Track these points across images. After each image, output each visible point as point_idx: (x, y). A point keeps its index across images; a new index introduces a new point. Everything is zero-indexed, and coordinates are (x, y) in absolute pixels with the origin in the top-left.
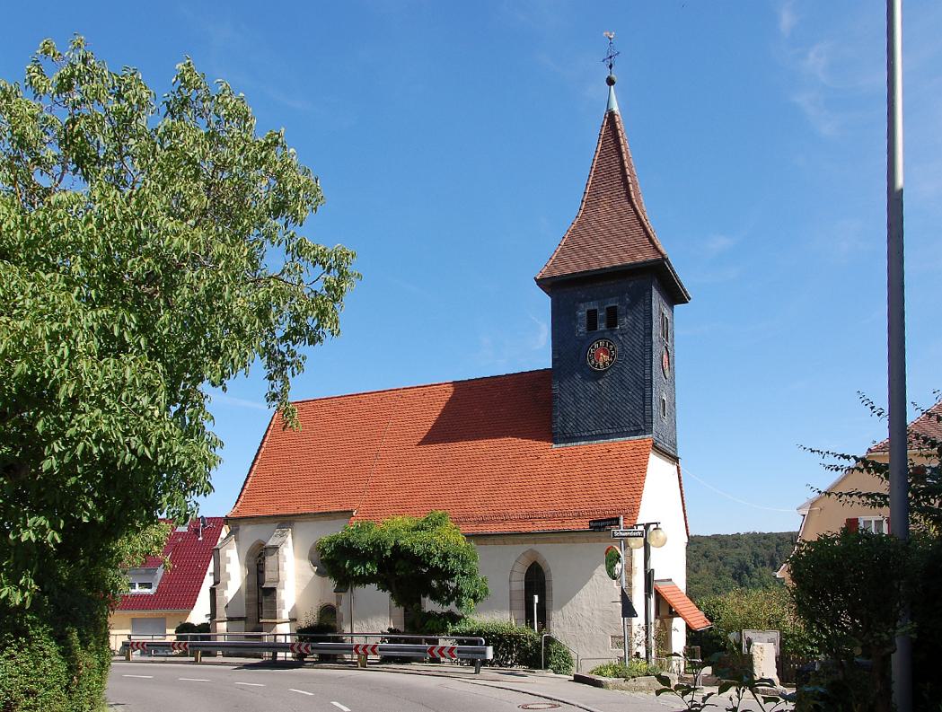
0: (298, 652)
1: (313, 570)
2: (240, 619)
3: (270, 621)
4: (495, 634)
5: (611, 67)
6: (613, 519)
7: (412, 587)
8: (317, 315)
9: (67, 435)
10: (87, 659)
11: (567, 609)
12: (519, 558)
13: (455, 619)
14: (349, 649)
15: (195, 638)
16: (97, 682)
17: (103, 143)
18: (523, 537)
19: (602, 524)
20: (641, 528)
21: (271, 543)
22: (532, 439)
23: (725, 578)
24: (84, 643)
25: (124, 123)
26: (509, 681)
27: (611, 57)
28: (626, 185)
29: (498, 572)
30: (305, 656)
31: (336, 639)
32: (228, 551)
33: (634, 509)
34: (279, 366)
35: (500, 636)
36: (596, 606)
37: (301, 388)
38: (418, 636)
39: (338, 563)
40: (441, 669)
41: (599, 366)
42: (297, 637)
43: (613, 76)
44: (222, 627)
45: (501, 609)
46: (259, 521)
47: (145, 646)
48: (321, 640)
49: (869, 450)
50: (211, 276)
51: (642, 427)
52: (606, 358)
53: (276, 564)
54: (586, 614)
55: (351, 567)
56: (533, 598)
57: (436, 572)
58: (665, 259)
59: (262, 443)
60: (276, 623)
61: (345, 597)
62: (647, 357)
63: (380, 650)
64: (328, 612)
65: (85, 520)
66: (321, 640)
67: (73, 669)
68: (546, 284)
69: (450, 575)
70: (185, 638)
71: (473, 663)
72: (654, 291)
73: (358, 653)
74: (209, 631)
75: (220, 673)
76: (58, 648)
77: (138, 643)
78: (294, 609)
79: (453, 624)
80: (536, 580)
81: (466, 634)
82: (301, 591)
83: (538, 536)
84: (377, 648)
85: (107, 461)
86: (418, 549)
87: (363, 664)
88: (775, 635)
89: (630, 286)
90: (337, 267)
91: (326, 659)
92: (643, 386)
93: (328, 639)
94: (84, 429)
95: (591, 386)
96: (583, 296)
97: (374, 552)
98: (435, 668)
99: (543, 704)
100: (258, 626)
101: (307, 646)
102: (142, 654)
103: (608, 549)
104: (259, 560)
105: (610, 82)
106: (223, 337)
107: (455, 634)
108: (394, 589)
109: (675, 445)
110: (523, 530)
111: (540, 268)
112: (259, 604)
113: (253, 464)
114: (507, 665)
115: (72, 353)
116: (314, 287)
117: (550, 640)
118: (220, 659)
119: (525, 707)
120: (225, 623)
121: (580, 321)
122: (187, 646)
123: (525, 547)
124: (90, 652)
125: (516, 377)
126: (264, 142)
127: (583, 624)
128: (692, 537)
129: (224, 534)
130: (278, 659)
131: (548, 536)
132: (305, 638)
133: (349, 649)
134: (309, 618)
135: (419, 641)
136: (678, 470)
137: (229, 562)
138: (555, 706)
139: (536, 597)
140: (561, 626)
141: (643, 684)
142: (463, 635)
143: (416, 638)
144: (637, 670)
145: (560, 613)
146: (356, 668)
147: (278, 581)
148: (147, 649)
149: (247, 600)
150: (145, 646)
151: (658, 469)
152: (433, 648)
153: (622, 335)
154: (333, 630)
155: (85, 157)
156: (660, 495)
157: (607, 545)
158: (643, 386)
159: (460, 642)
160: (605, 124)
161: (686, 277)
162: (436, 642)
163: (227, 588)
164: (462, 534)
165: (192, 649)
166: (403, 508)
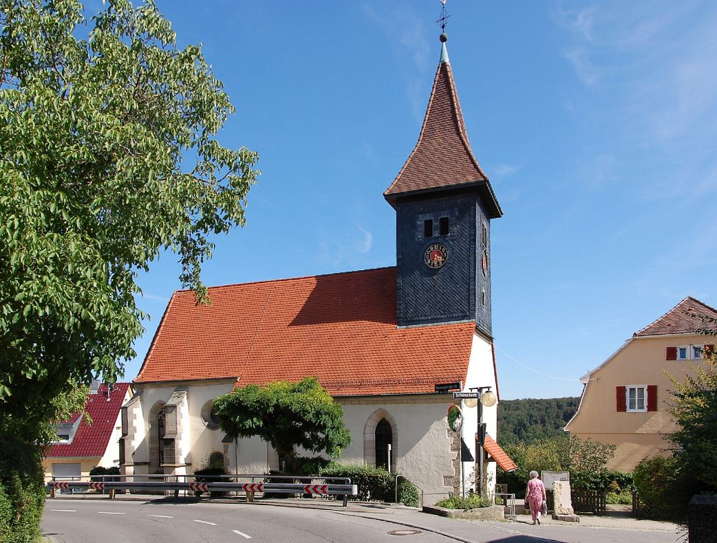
0: (196, 490)
1: (205, 425)
2: (145, 463)
3: (170, 465)
4: (357, 474)
5: (443, 27)
6: (453, 384)
7: (285, 439)
8: (226, 206)
9: (16, 299)
10: (27, 496)
11: (409, 455)
12: (371, 416)
13: (325, 463)
14: (239, 487)
15: (110, 479)
16: (35, 516)
17: (37, 47)
18: (376, 399)
19: (445, 388)
20: (476, 391)
21: (170, 402)
22: (381, 322)
23: (508, 433)
24: (25, 484)
25: (54, 34)
26: (372, 513)
27: (443, 19)
28: (456, 122)
29: (357, 426)
30: (202, 493)
31: (227, 480)
32: (134, 409)
33: (463, 377)
34: (191, 252)
35: (362, 476)
36: (432, 453)
37: (213, 274)
38: (291, 476)
39: (228, 419)
40: (313, 503)
41: (434, 264)
42: (195, 478)
43: (445, 34)
44: (130, 470)
45: (356, 456)
46: (161, 388)
47: (67, 485)
48: (213, 480)
49: (635, 334)
50: (138, 164)
51: (468, 313)
52: (440, 259)
53: (174, 421)
54: (426, 457)
55: (241, 421)
56: (387, 447)
57: (309, 426)
58: (486, 181)
59: (161, 323)
60: (175, 467)
61: (231, 446)
62: (472, 270)
63: (105, 486)
64: (217, 458)
65: (29, 376)
66: (213, 480)
67: (17, 505)
68: (395, 199)
69: (322, 428)
70: (100, 479)
71: (340, 498)
72: (478, 208)
73: (247, 491)
74: (119, 473)
75: (129, 507)
76: (4, 488)
77: (61, 483)
78: (189, 455)
79: (323, 467)
80: (384, 435)
81: (334, 475)
82: (195, 441)
83: (387, 398)
84: (263, 486)
85: (52, 321)
86: (295, 407)
87: (251, 500)
88: (566, 475)
89: (459, 202)
90: (242, 165)
91: (218, 495)
92: (468, 281)
93: (220, 480)
94: (31, 294)
95: (427, 280)
96: (421, 209)
97: (260, 409)
98: (309, 502)
99: (408, 531)
100: (160, 469)
101: (205, 485)
102: (62, 492)
103: (450, 409)
104: (160, 417)
105: (443, 39)
106: (151, 220)
107: (325, 475)
108: (275, 439)
109: (491, 328)
110: (374, 393)
111: (388, 186)
112: (161, 453)
113: (154, 339)
114: (365, 499)
115: (21, 226)
116: (223, 184)
117: (401, 480)
118: (128, 495)
119: (393, 533)
120: (132, 467)
121: (419, 229)
122: (103, 485)
123: (376, 407)
124: (29, 491)
125: (379, 271)
126: (183, 55)
127: (422, 467)
128: (502, 401)
129: (128, 396)
130: (179, 495)
131: (395, 398)
132: (201, 478)
133: (239, 487)
134: (201, 463)
135: (291, 481)
136: (493, 349)
137: (135, 418)
138: (417, 532)
139: (390, 445)
140: (405, 466)
141: (478, 514)
142: (334, 475)
143: (288, 479)
144: (473, 503)
145: (404, 458)
146: (245, 503)
147: (176, 433)
148: (68, 488)
149: (151, 449)
150: (67, 485)
151: (479, 346)
152: (308, 486)
153: (452, 240)
154: (222, 471)
155: (22, 61)
156: (479, 368)
157: (449, 405)
158: (468, 281)
159: (329, 481)
160: (439, 73)
161: (501, 197)
162: (309, 481)
163: (134, 439)
164: (331, 396)
165: (107, 488)
166: (280, 376)
